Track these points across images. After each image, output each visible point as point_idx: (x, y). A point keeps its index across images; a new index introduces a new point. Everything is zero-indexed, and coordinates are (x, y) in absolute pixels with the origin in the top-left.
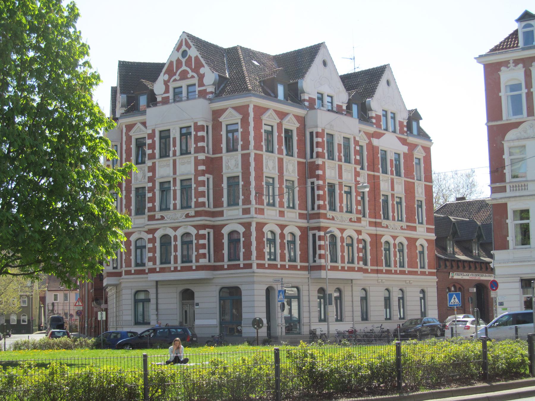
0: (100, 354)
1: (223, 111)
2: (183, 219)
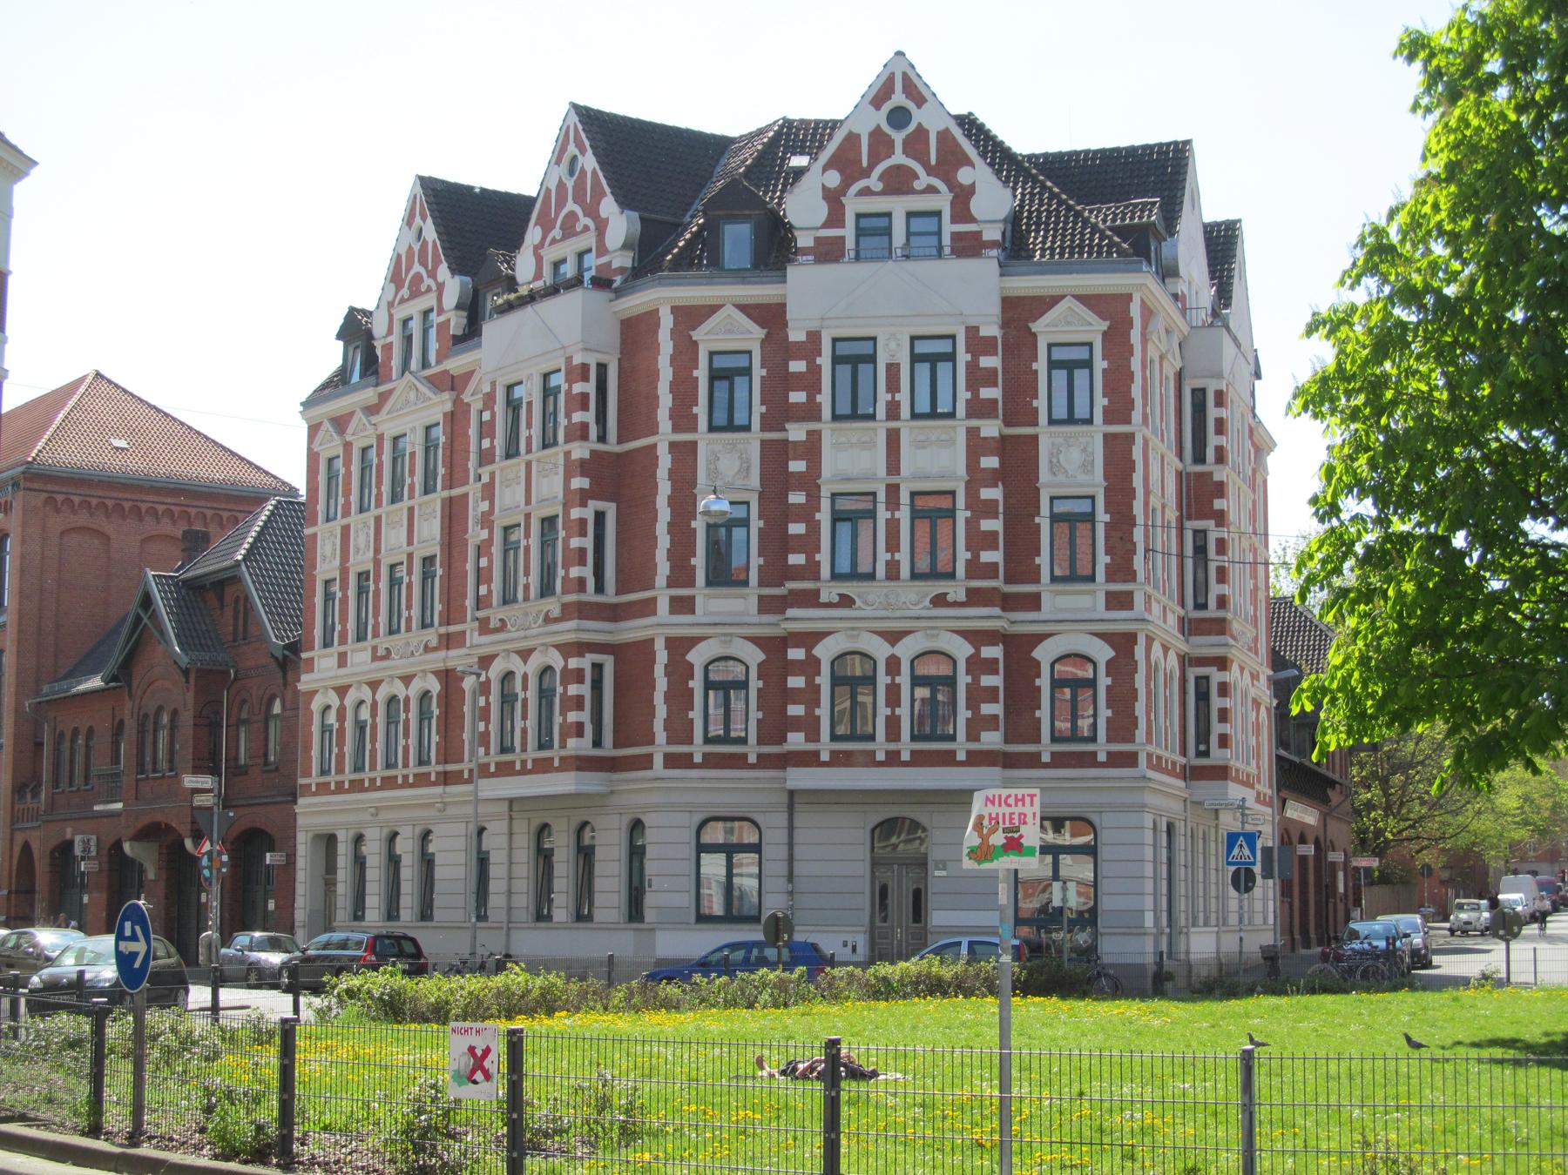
1: (1045, 303)
2: (923, 608)
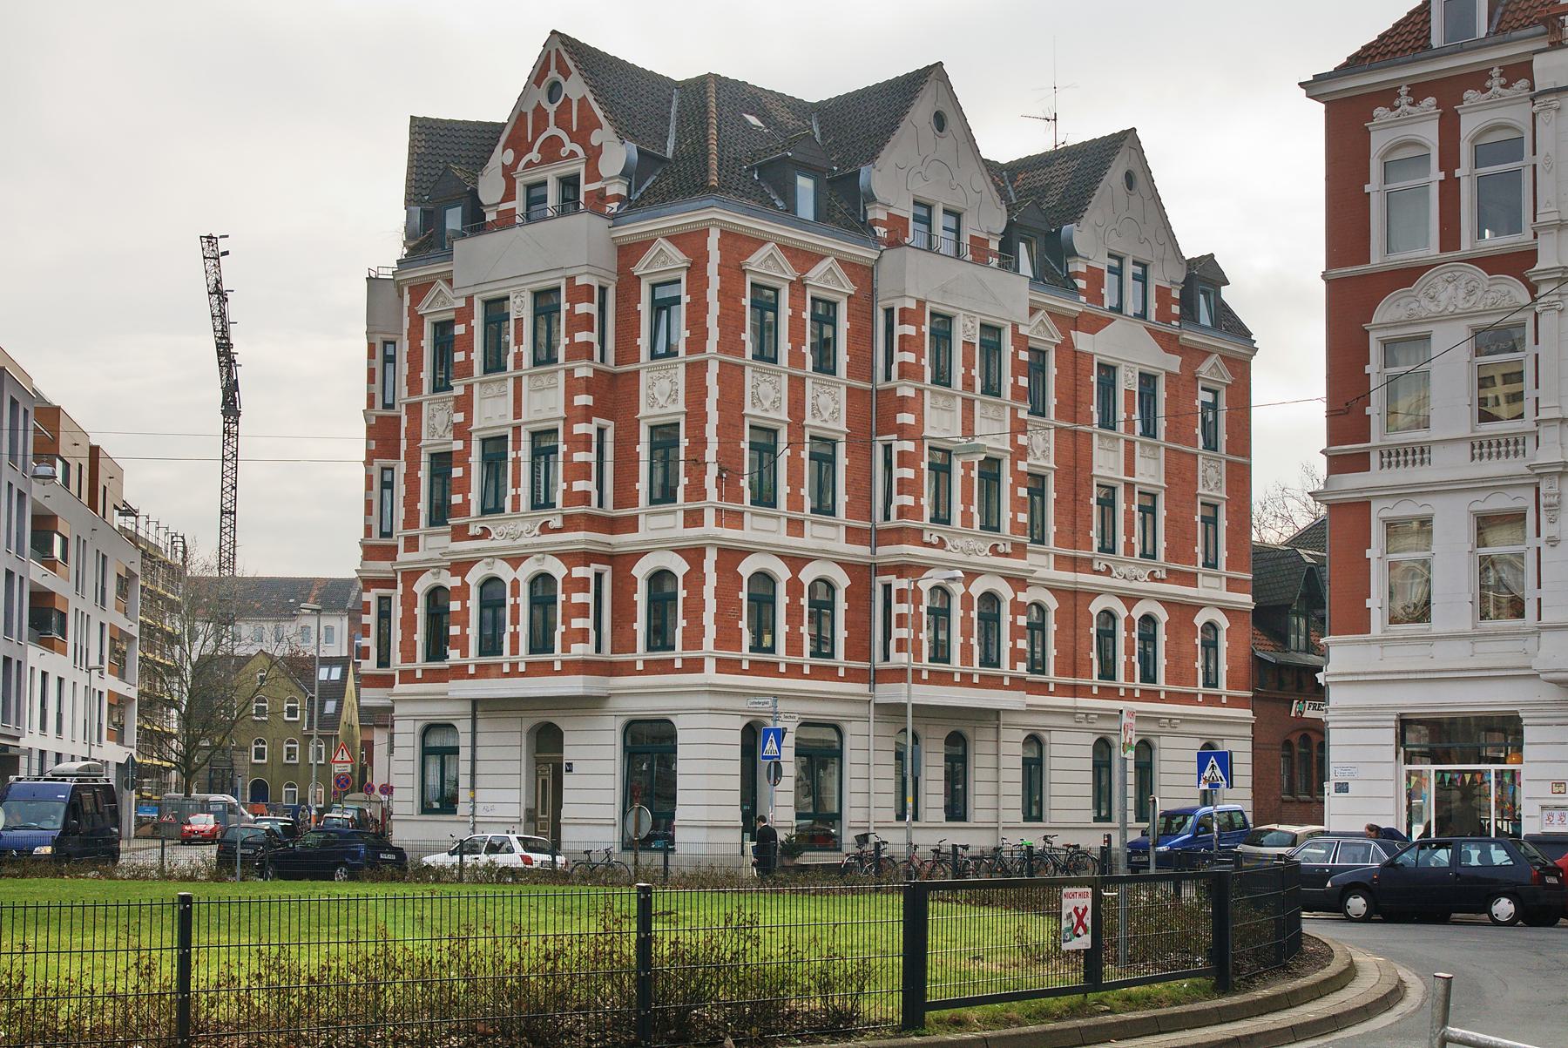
0: (374, 892)
1: (644, 245)
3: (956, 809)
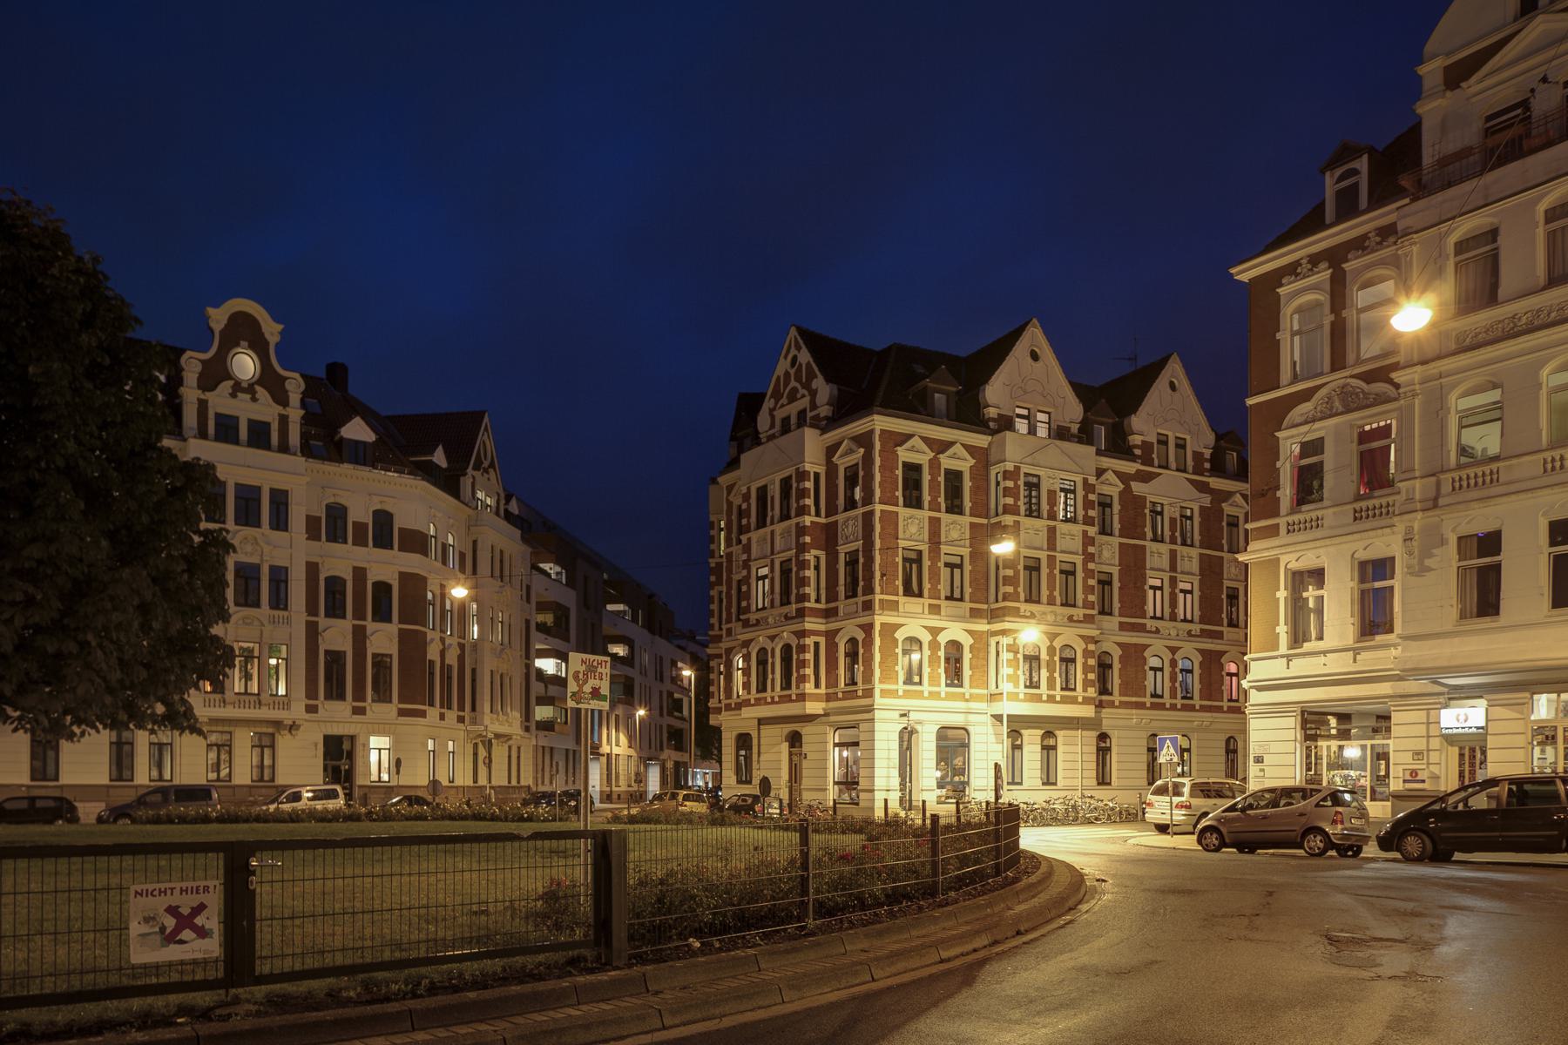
3: (1049, 780)
